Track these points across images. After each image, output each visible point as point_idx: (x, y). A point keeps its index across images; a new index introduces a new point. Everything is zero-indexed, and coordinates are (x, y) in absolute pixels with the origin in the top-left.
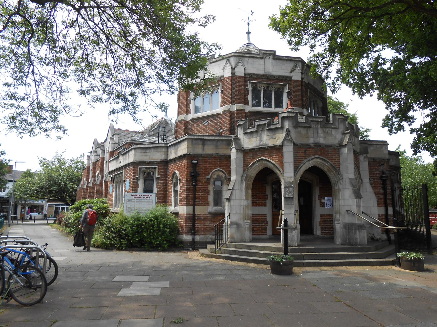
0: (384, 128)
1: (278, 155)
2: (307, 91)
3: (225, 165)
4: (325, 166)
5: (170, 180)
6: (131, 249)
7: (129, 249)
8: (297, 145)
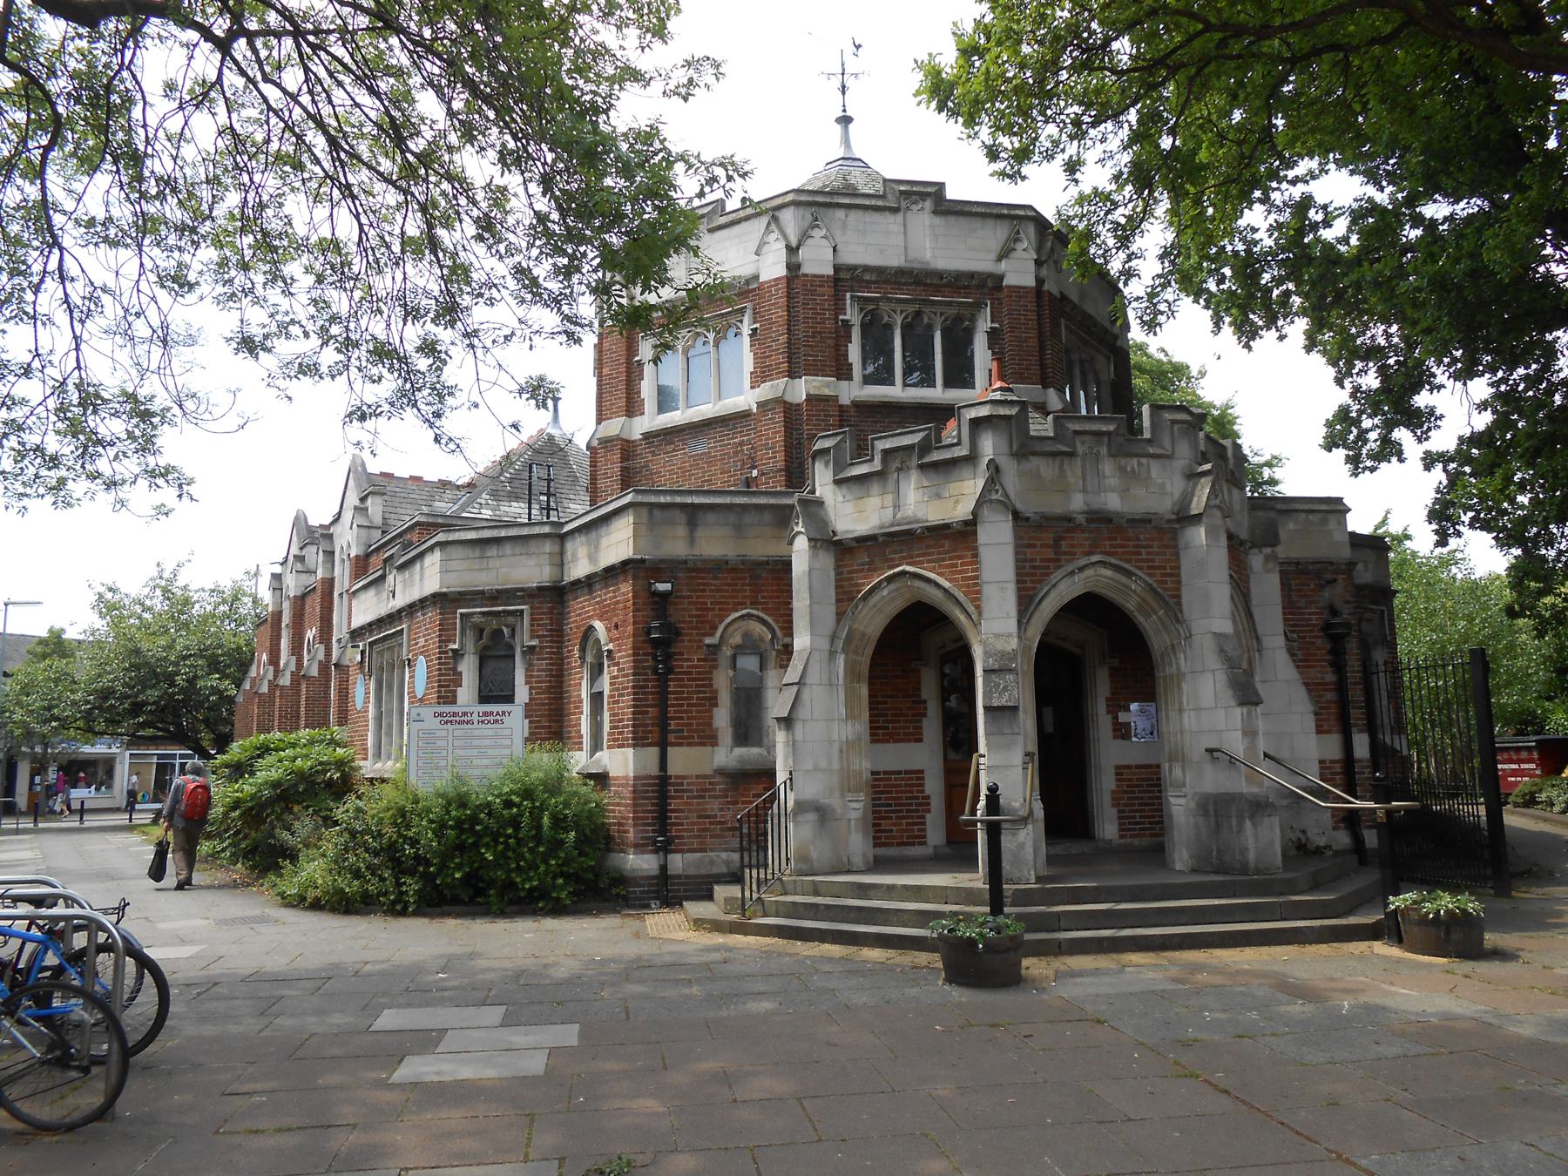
1: (959, 557)
2: (1058, 325)
3: (771, 598)
4: (1129, 593)
5: (572, 656)
6: (465, 909)
7: (429, 910)
8: (1028, 519)
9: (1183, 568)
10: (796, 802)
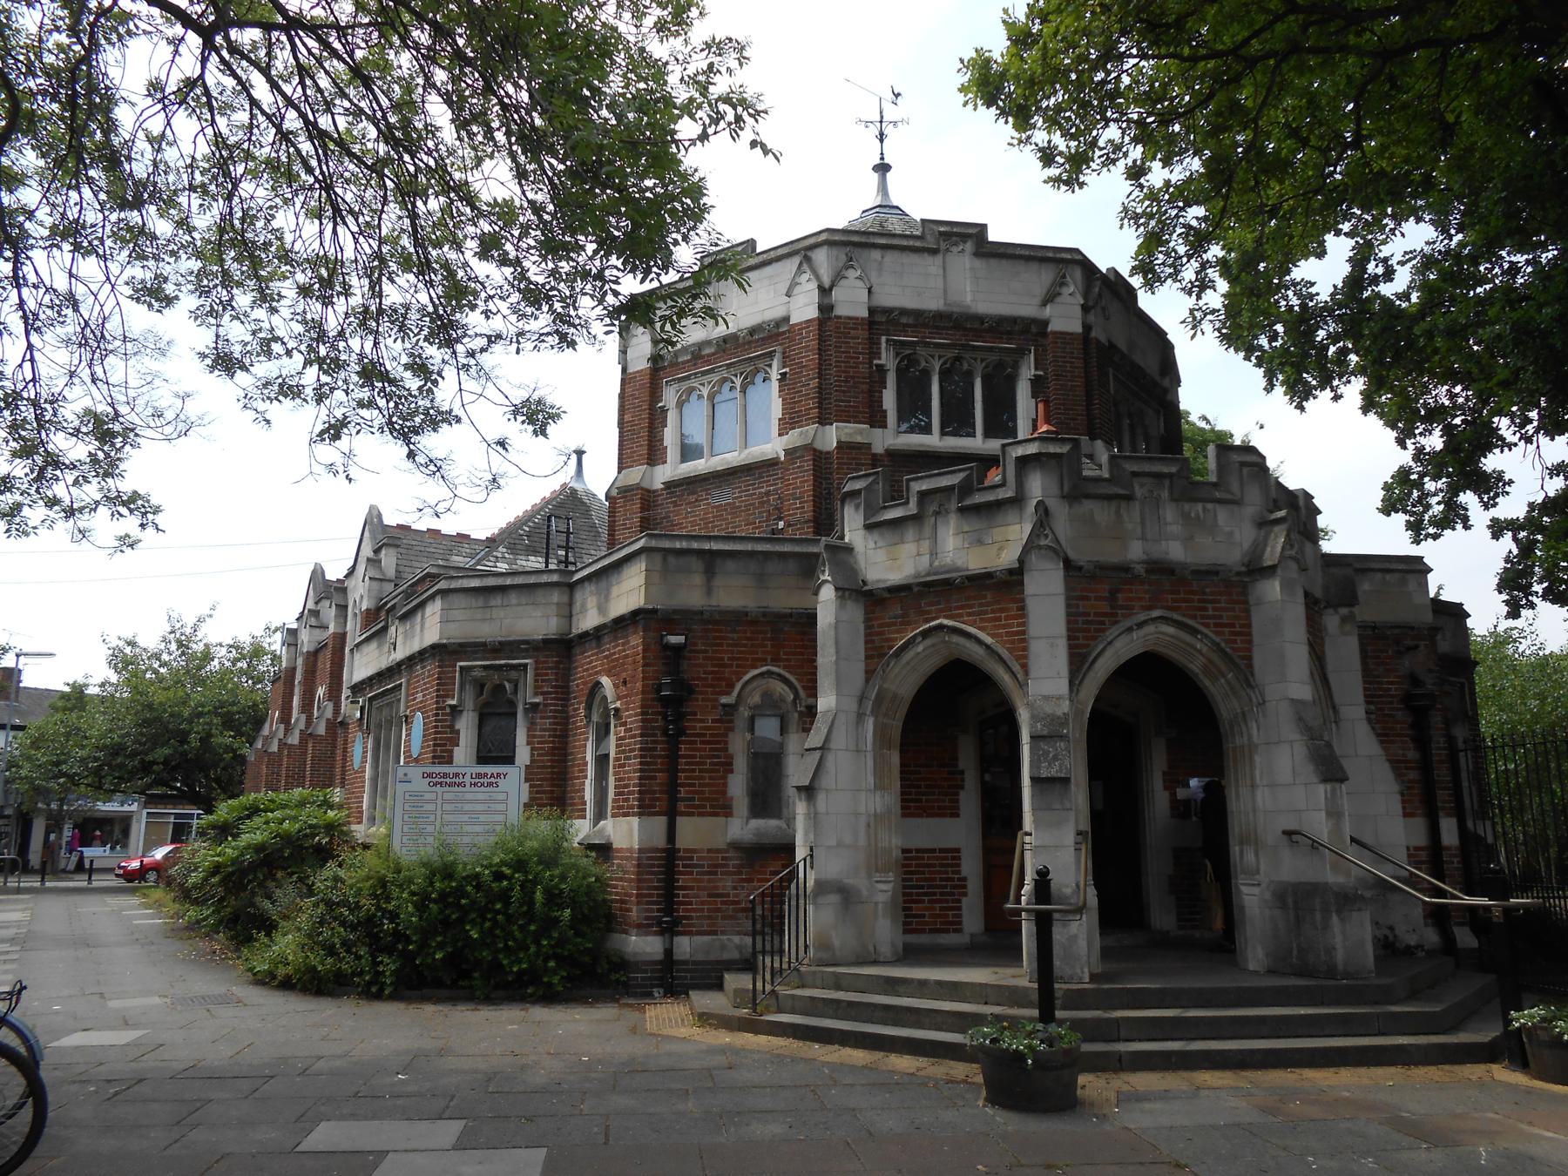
1: (1002, 610)
3: (793, 654)
5: (578, 715)
8: (1080, 568)
10: (816, 881)
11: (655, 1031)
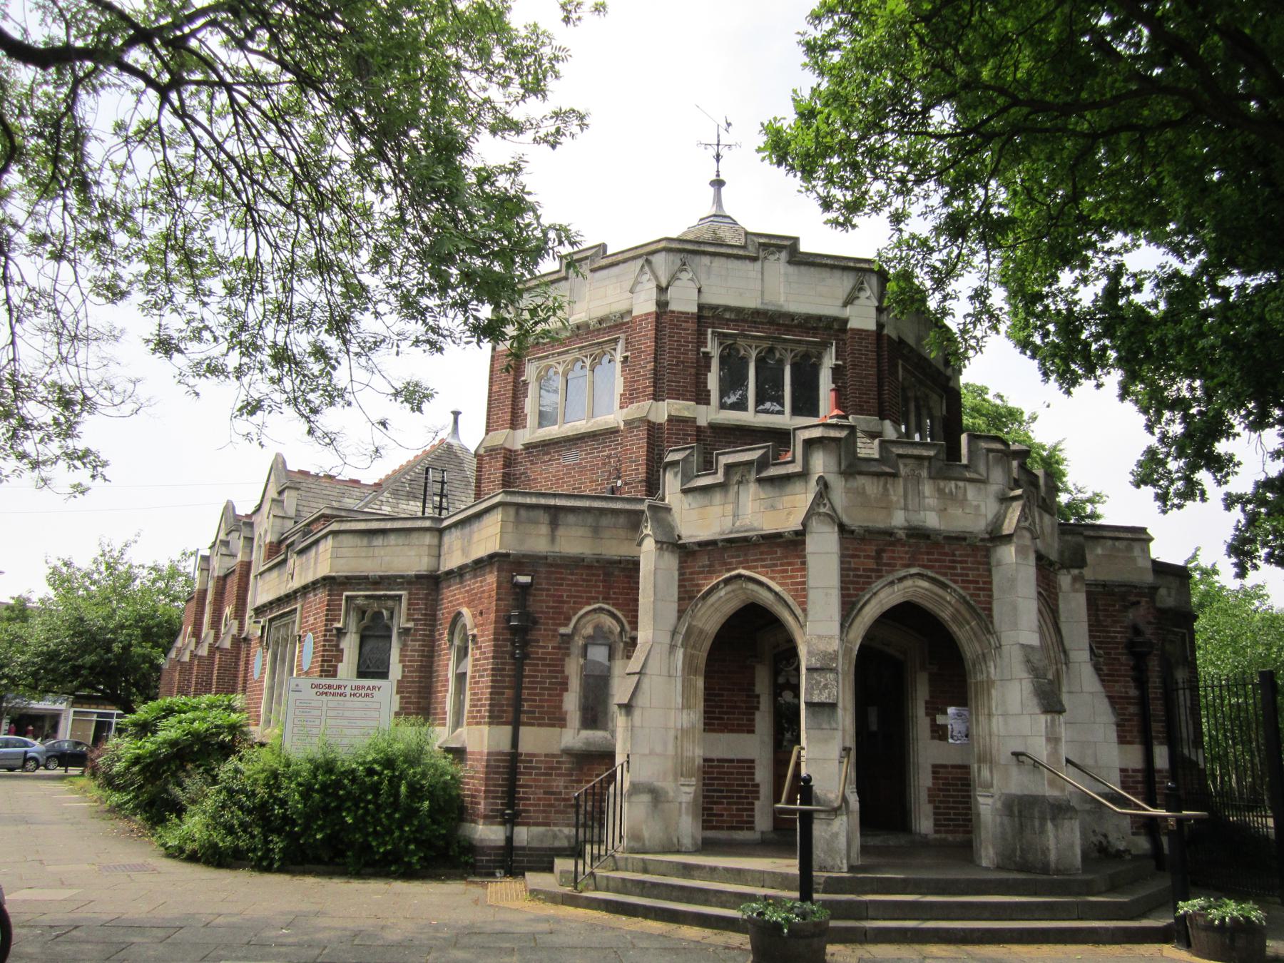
0: (1138, 486)
1: (789, 564)
7: (292, 867)
8: (852, 532)
9: (995, 583)
11: (493, 902)
